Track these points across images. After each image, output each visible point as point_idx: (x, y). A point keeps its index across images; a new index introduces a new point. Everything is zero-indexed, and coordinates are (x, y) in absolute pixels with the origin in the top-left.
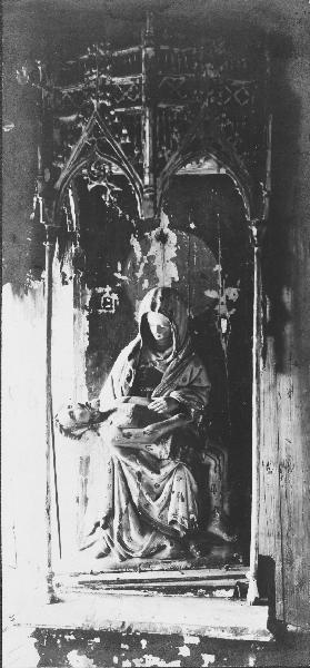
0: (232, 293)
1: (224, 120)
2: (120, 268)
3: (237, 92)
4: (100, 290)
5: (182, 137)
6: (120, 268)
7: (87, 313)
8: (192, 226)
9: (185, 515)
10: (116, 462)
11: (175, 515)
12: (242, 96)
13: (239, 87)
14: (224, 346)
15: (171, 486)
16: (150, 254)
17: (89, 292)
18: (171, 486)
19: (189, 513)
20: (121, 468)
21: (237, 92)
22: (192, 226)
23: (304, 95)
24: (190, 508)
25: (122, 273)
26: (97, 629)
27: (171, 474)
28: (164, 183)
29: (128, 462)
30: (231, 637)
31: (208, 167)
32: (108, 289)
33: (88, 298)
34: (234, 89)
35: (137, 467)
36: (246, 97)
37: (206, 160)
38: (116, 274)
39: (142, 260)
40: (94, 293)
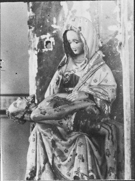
4: (43, 37)
7: (36, 52)
9: (85, 173)
10: (38, 133)
11: (77, 172)
15: (74, 150)
16: (73, 9)
18: (74, 150)
19: (88, 172)
20: (41, 138)
23: (25, 3)
24: (90, 168)
25: (56, 24)
27: (74, 141)
29: (45, 133)
30: (130, 131)
31: (115, 117)
32: (49, 35)
37: (115, 47)
38: (52, 26)
39: (68, 14)
40: (40, 39)
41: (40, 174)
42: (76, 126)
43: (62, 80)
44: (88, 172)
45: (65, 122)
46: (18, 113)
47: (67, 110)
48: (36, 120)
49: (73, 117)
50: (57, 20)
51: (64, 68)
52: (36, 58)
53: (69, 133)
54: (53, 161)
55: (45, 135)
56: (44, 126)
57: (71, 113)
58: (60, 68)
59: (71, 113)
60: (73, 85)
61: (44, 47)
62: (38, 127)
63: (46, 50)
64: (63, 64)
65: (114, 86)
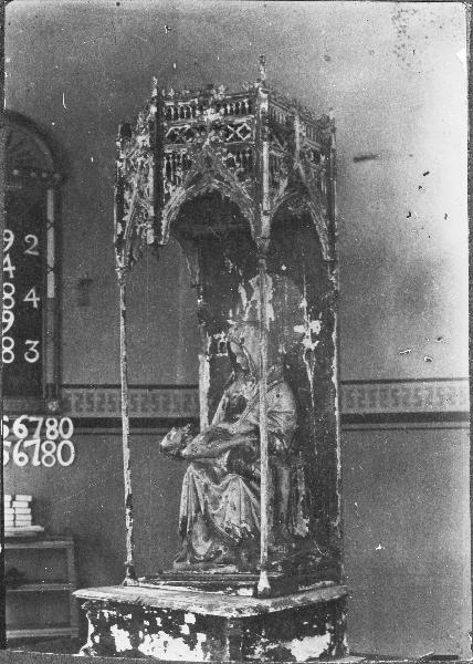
0: (316, 326)
1: (226, 155)
2: (231, 315)
3: (239, 129)
4: (217, 336)
5: (185, 174)
6: (231, 315)
8: (284, 268)
12: (244, 132)
13: (240, 125)
14: (310, 378)
16: (253, 299)
17: (209, 339)
19: (241, 522)
21: (239, 129)
22: (284, 268)
25: (233, 319)
26: (119, 601)
28: (169, 214)
33: (209, 345)
34: (236, 127)
35: (206, 480)
36: (248, 132)
40: (213, 339)
41: (191, 526)
42: (229, 465)
43: (229, 403)
44: (241, 522)
45: (218, 462)
46: (172, 448)
47: (221, 446)
48: (190, 459)
49: (227, 455)
50: (234, 312)
51: (232, 388)
52: (207, 365)
53: (225, 474)
54: (205, 510)
55: (198, 477)
56: (199, 466)
57: (225, 451)
58: (227, 387)
59: (225, 451)
60: (241, 411)
61: (63, 592)
62: (191, 467)
63: (221, 355)
64: (231, 382)
65: (290, 413)
